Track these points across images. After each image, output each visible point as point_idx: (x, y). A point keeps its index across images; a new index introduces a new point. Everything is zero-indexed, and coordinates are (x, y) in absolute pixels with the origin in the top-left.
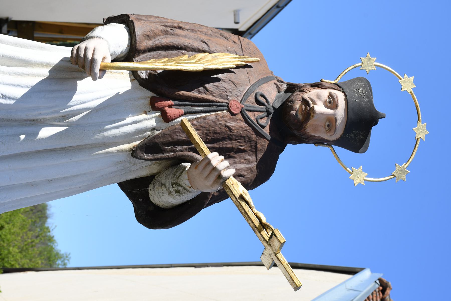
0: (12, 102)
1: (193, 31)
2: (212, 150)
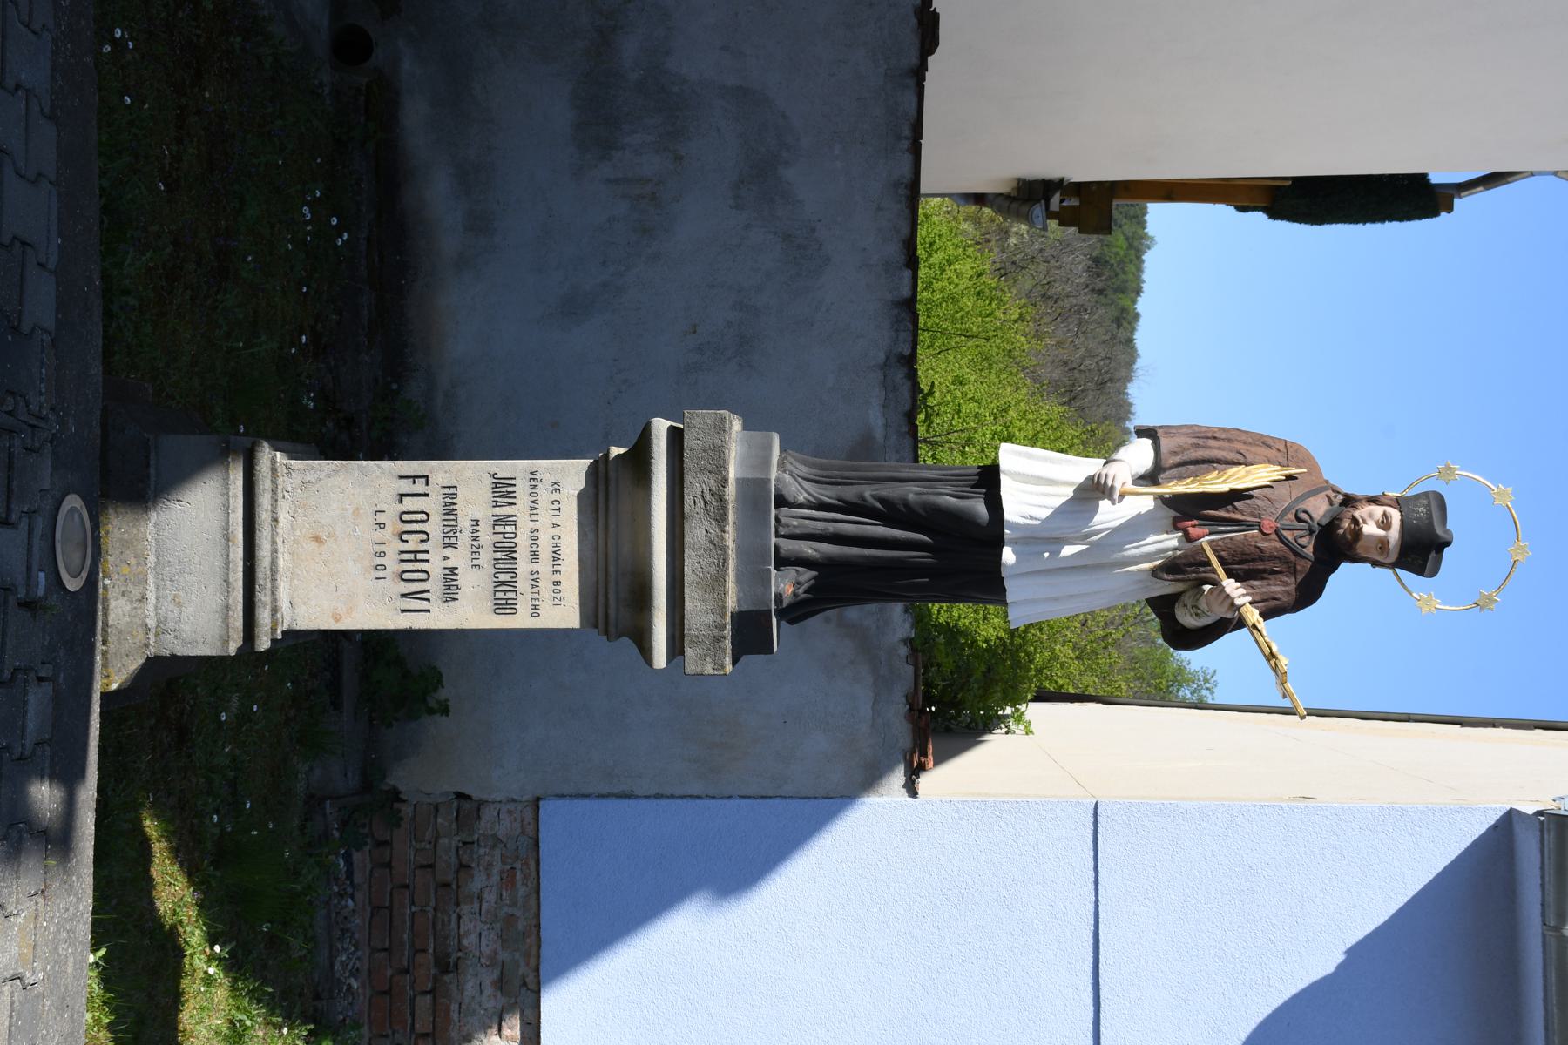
0: (1038, 522)
1: (1229, 440)
2: (1230, 574)
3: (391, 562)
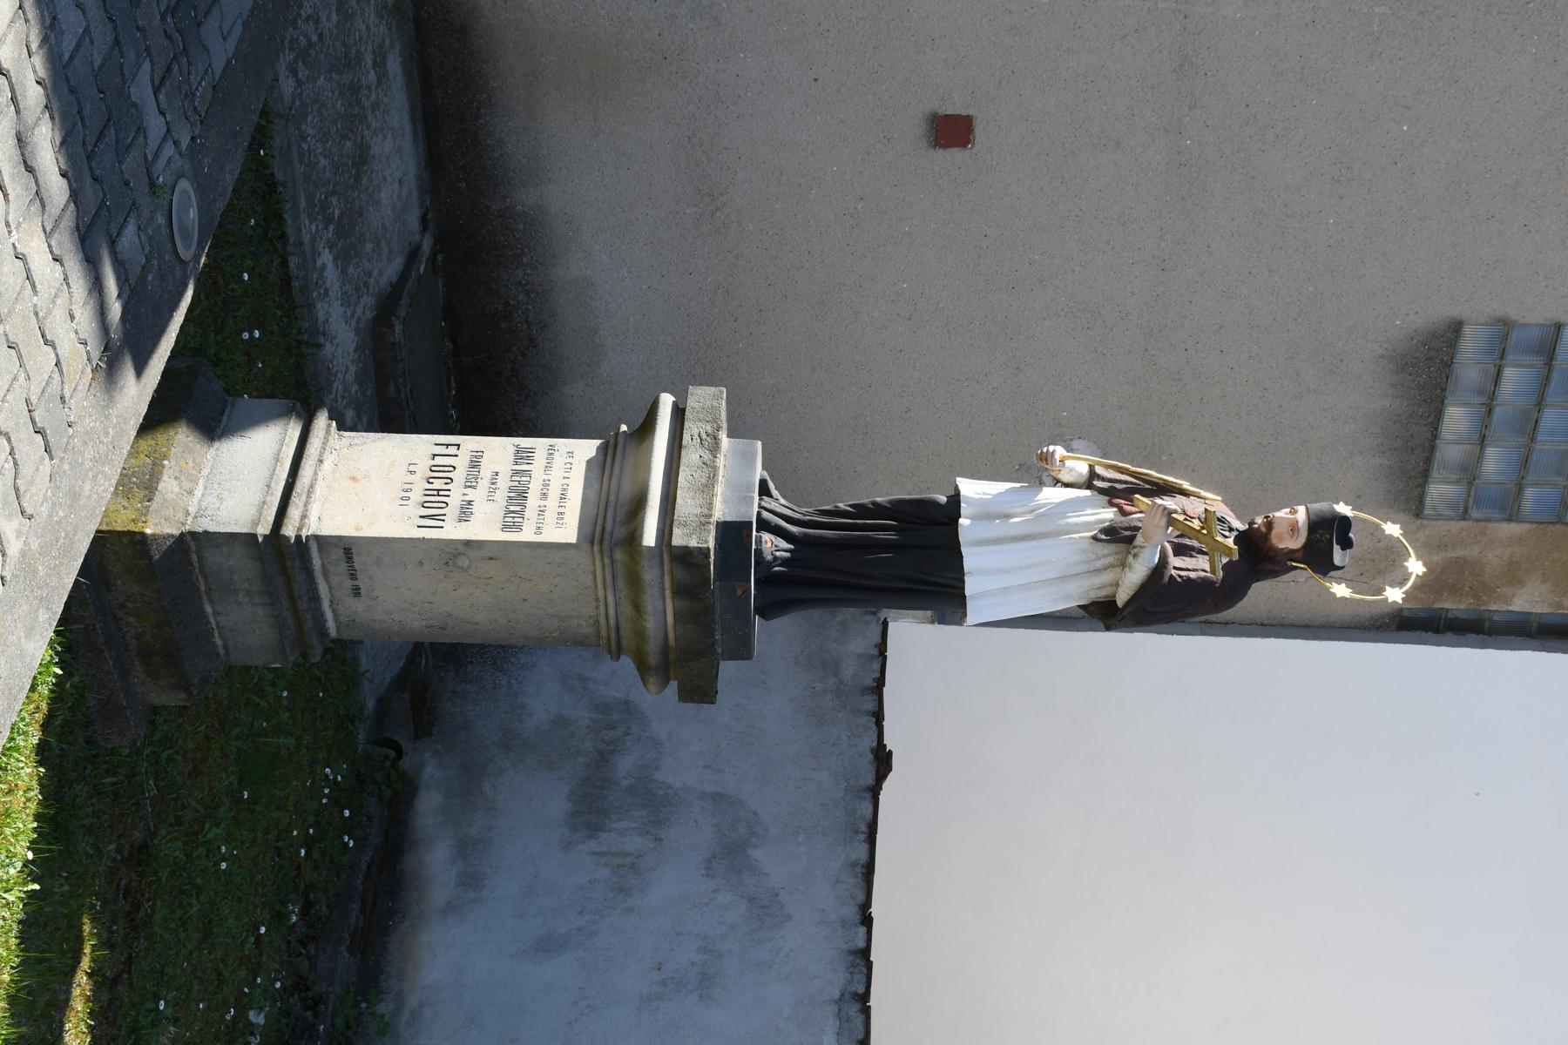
0: (990, 497)
3: (417, 495)
